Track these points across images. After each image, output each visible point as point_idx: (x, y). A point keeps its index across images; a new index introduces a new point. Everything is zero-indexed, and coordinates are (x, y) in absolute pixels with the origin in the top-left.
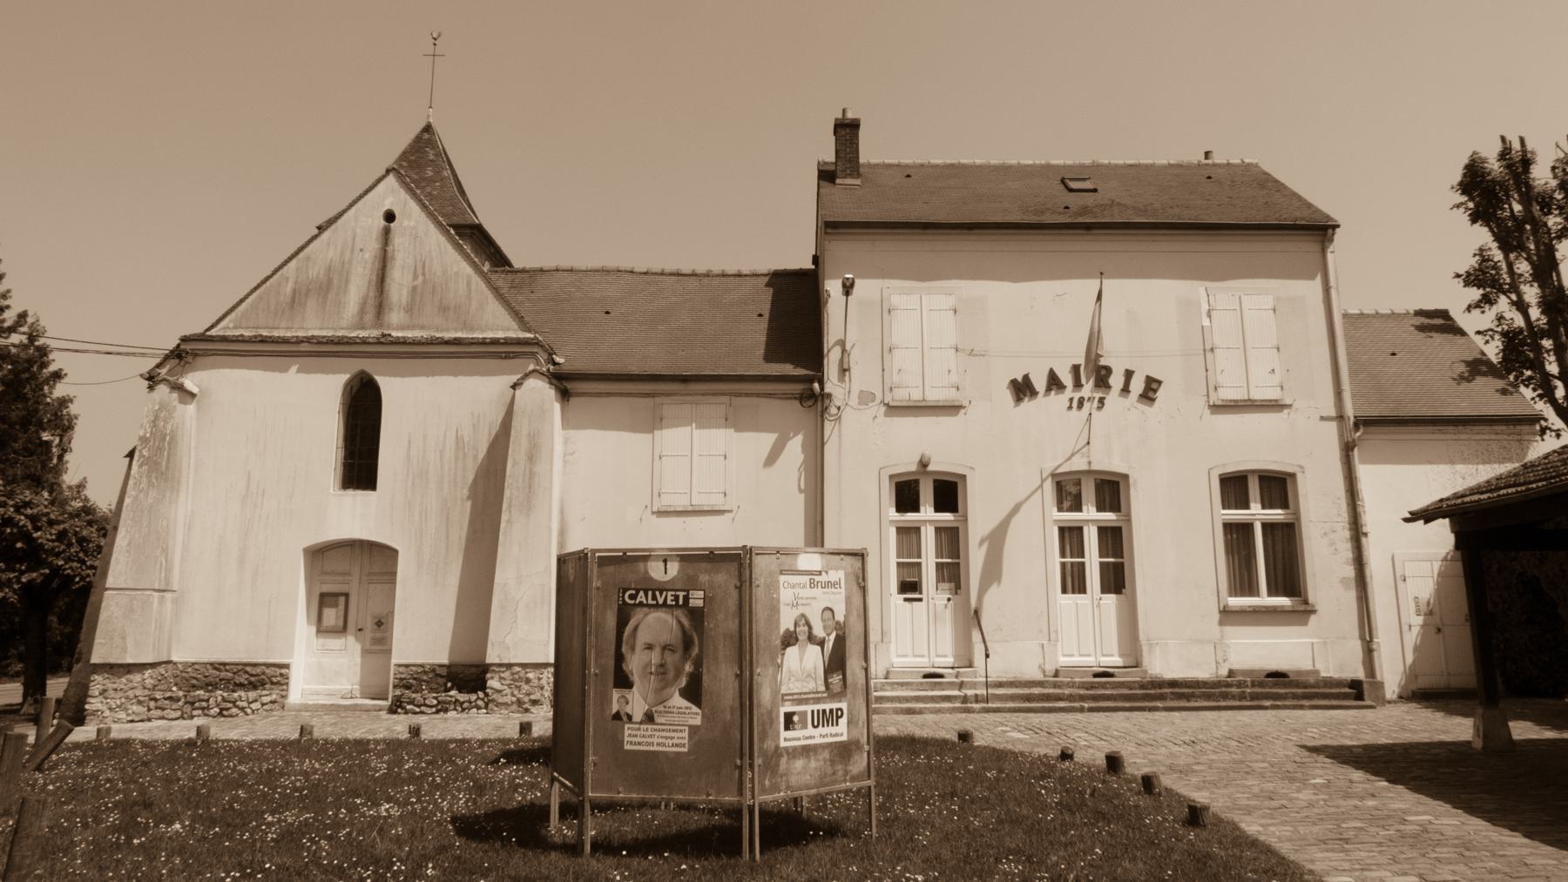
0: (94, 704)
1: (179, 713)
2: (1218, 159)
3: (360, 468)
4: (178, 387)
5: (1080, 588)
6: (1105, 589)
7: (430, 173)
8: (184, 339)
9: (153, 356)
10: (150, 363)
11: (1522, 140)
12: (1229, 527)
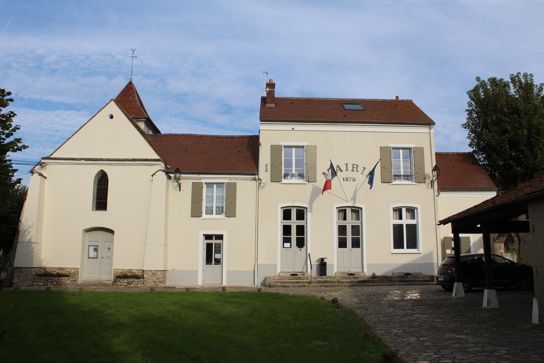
0: (15, 280)
1: (43, 284)
2: (400, 98)
3: (101, 202)
4: (41, 175)
5: (345, 246)
6: (353, 246)
7: (131, 99)
8: (43, 158)
9: (32, 165)
10: (32, 167)
11: (27, 219)
12: (208, 244)
